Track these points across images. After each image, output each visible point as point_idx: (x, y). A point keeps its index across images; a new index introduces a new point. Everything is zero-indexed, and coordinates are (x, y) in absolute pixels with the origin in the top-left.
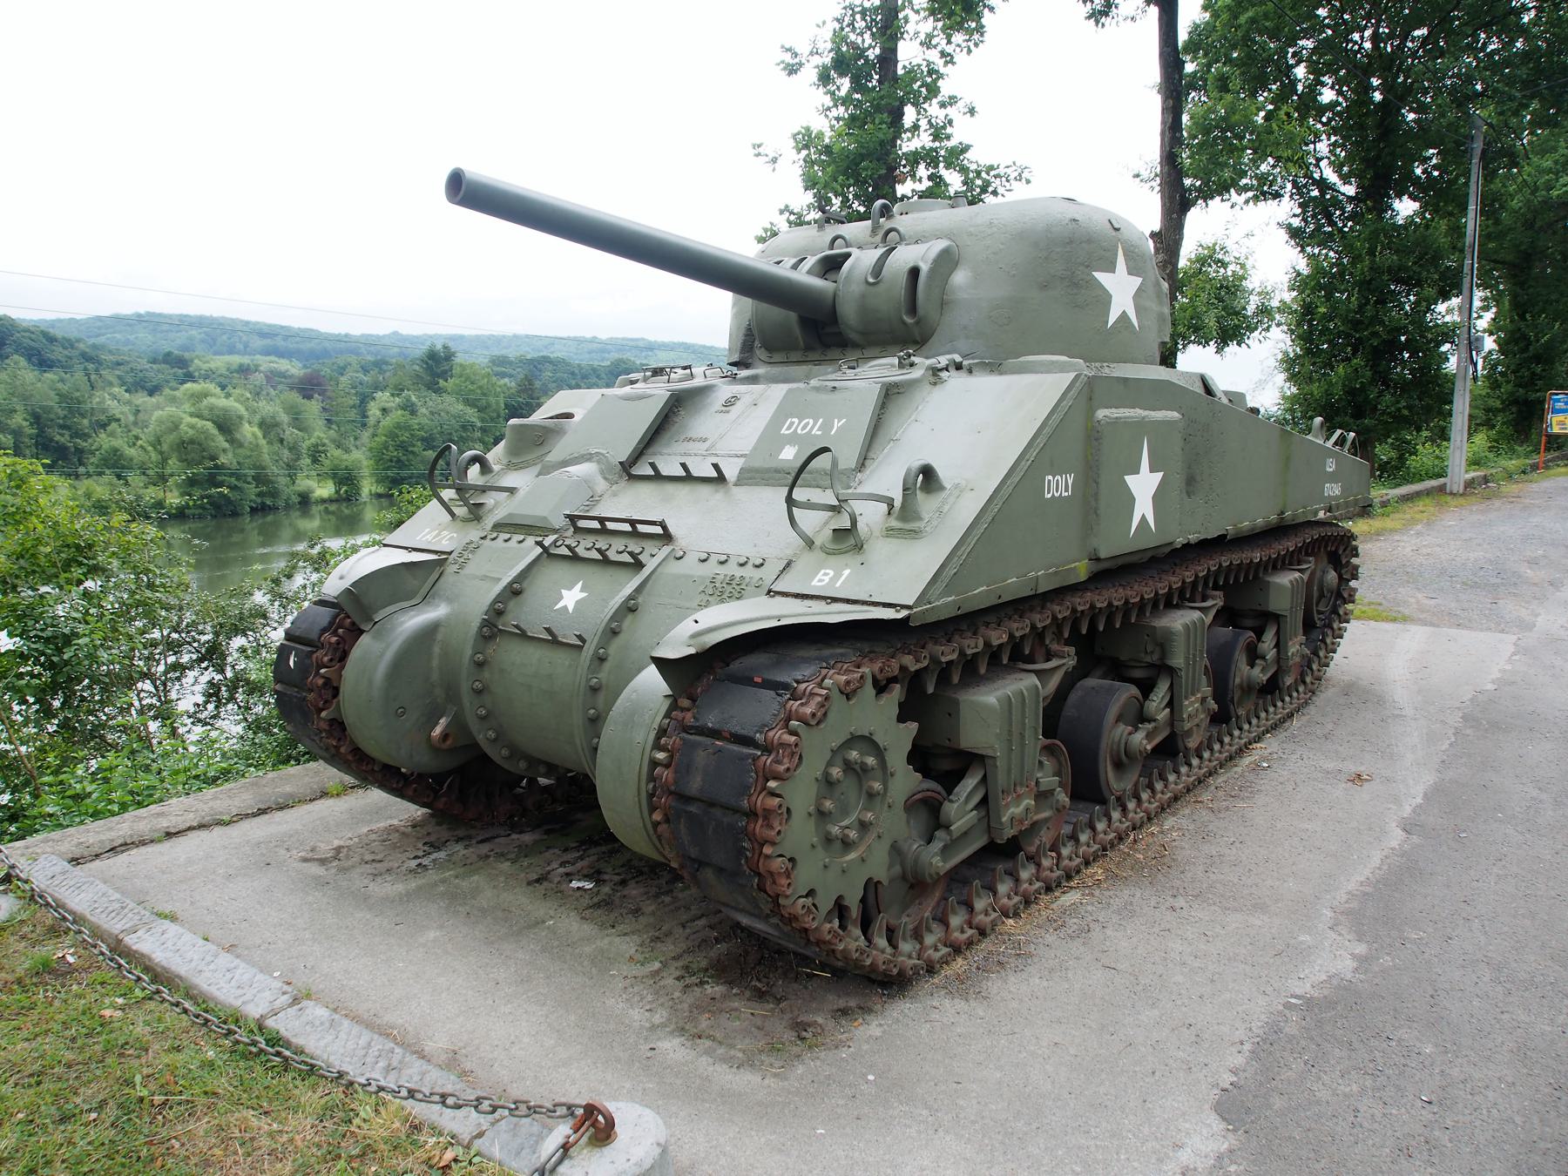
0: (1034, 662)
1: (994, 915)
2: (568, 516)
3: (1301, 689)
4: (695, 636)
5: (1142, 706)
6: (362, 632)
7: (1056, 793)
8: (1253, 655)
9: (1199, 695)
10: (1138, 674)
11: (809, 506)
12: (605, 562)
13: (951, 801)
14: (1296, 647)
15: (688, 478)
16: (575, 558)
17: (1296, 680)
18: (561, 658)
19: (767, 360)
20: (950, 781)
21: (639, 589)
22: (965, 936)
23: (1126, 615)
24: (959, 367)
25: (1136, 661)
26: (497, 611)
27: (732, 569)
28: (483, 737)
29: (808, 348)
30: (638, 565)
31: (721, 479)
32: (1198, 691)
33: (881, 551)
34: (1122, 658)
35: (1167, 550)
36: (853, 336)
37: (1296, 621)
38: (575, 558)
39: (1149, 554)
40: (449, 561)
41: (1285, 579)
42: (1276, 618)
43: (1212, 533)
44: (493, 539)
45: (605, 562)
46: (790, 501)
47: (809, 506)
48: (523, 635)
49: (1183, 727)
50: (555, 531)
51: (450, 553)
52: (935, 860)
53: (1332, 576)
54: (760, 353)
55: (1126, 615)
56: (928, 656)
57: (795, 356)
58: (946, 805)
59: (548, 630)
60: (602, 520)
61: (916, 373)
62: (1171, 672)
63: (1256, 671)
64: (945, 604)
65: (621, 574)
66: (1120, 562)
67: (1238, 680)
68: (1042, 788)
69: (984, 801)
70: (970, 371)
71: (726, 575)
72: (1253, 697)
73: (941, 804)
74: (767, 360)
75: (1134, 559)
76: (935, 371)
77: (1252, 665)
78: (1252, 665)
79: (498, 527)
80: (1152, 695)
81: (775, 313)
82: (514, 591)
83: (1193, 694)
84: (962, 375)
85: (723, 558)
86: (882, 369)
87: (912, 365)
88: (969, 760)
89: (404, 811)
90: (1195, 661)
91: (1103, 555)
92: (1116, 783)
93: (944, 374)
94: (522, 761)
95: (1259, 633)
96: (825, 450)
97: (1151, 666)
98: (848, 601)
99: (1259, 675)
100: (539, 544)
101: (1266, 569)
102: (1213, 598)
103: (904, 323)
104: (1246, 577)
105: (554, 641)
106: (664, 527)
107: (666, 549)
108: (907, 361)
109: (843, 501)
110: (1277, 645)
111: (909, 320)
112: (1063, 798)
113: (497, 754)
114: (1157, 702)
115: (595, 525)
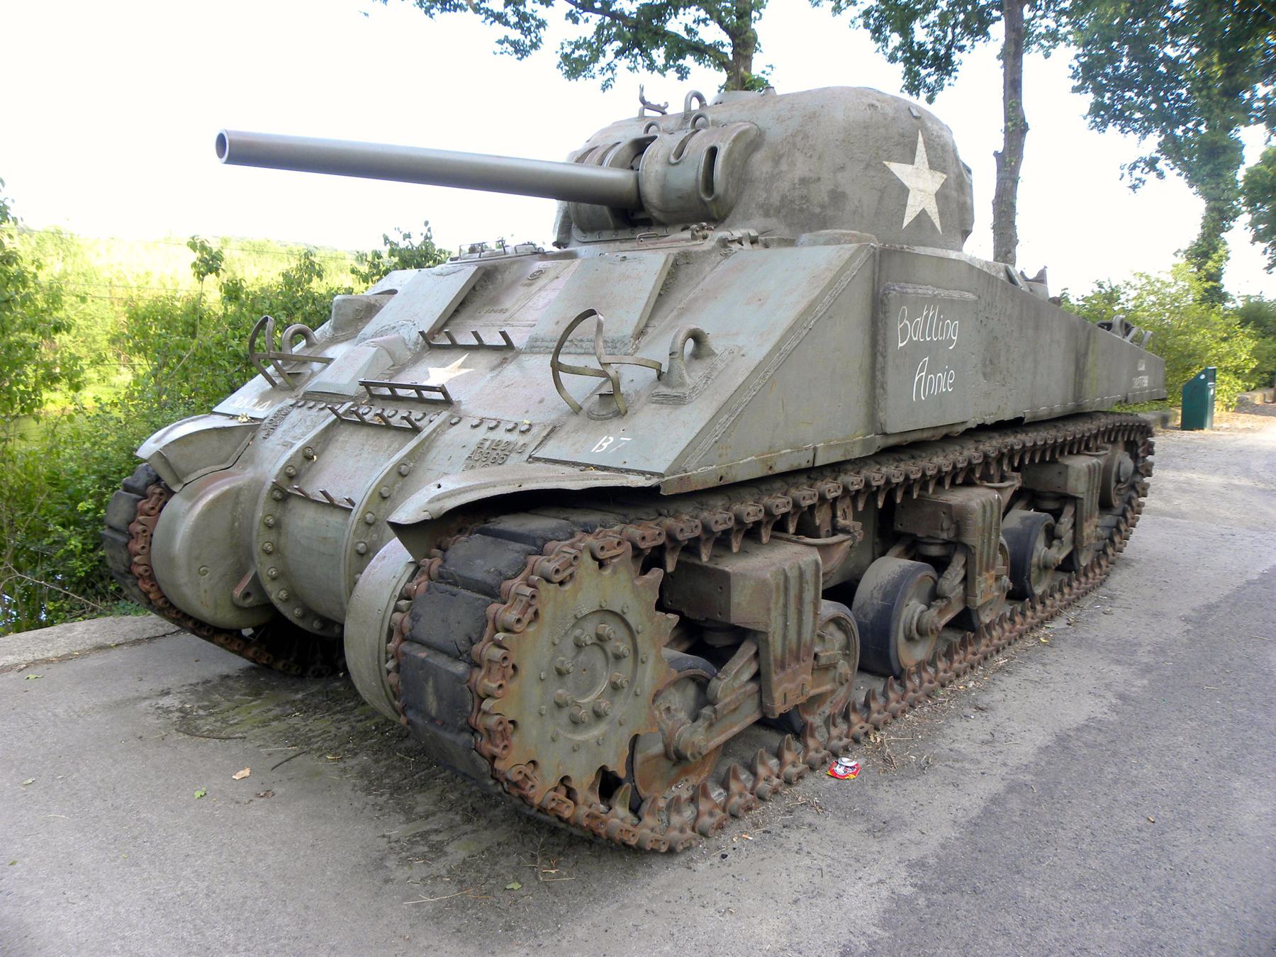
0: (819, 537)
1: (845, 741)
2: (363, 383)
3: (1097, 571)
4: (438, 499)
5: (936, 583)
6: (172, 493)
7: (838, 666)
8: (1052, 536)
9: (993, 572)
10: (935, 551)
11: (572, 370)
12: (388, 427)
13: (719, 679)
14: (1093, 528)
15: (481, 347)
16: (363, 423)
17: (1092, 562)
18: (335, 518)
19: (583, 239)
20: (719, 658)
21: (411, 455)
22: (820, 756)
23: (908, 492)
24: (754, 241)
25: (933, 538)
26: (291, 475)
27: (500, 435)
28: (276, 594)
29: (617, 228)
30: (416, 430)
31: (509, 346)
32: (993, 568)
33: (648, 418)
34: (919, 535)
35: (961, 429)
36: (656, 214)
37: (1090, 502)
38: (363, 423)
39: (945, 431)
40: (262, 427)
41: (1080, 464)
42: (1073, 500)
43: (1008, 416)
44: (311, 408)
45: (388, 427)
46: (556, 367)
47: (572, 370)
48: (307, 499)
49: (975, 602)
50: (351, 398)
51: (263, 420)
52: (698, 738)
53: (1128, 464)
54: (576, 233)
55: (908, 492)
56: (700, 526)
57: (607, 235)
58: (714, 683)
59: (324, 493)
60: (419, 389)
61: (708, 245)
62: (967, 549)
63: (1054, 550)
64: (703, 473)
65: (400, 437)
66: (911, 438)
67: (1035, 560)
68: (823, 661)
69: (756, 677)
70: (766, 246)
71: (493, 441)
72: (1050, 573)
73: (709, 681)
74: (583, 239)
75: (925, 435)
76: (725, 243)
77: (1049, 546)
78: (1049, 546)
79: (309, 396)
80: (946, 573)
81: (641, 216)
82: (307, 456)
83: (987, 570)
84: (758, 251)
85: (493, 424)
86: (680, 240)
87: (705, 237)
88: (741, 634)
89: (235, 663)
90: (989, 540)
91: (889, 430)
92: (910, 655)
93: (735, 247)
94: (316, 622)
95: (1057, 514)
96: (591, 313)
97: (946, 543)
98: (597, 468)
99: (1058, 554)
100: (334, 412)
101: (1062, 453)
102: (1012, 478)
103: (702, 201)
104: (1032, 460)
105: (331, 505)
106: (445, 393)
107: (445, 414)
108: (700, 234)
109: (605, 364)
110: (1074, 526)
111: (708, 199)
112: (844, 667)
113: (292, 613)
114: (952, 579)
115: (412, 393)
